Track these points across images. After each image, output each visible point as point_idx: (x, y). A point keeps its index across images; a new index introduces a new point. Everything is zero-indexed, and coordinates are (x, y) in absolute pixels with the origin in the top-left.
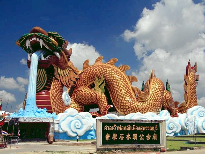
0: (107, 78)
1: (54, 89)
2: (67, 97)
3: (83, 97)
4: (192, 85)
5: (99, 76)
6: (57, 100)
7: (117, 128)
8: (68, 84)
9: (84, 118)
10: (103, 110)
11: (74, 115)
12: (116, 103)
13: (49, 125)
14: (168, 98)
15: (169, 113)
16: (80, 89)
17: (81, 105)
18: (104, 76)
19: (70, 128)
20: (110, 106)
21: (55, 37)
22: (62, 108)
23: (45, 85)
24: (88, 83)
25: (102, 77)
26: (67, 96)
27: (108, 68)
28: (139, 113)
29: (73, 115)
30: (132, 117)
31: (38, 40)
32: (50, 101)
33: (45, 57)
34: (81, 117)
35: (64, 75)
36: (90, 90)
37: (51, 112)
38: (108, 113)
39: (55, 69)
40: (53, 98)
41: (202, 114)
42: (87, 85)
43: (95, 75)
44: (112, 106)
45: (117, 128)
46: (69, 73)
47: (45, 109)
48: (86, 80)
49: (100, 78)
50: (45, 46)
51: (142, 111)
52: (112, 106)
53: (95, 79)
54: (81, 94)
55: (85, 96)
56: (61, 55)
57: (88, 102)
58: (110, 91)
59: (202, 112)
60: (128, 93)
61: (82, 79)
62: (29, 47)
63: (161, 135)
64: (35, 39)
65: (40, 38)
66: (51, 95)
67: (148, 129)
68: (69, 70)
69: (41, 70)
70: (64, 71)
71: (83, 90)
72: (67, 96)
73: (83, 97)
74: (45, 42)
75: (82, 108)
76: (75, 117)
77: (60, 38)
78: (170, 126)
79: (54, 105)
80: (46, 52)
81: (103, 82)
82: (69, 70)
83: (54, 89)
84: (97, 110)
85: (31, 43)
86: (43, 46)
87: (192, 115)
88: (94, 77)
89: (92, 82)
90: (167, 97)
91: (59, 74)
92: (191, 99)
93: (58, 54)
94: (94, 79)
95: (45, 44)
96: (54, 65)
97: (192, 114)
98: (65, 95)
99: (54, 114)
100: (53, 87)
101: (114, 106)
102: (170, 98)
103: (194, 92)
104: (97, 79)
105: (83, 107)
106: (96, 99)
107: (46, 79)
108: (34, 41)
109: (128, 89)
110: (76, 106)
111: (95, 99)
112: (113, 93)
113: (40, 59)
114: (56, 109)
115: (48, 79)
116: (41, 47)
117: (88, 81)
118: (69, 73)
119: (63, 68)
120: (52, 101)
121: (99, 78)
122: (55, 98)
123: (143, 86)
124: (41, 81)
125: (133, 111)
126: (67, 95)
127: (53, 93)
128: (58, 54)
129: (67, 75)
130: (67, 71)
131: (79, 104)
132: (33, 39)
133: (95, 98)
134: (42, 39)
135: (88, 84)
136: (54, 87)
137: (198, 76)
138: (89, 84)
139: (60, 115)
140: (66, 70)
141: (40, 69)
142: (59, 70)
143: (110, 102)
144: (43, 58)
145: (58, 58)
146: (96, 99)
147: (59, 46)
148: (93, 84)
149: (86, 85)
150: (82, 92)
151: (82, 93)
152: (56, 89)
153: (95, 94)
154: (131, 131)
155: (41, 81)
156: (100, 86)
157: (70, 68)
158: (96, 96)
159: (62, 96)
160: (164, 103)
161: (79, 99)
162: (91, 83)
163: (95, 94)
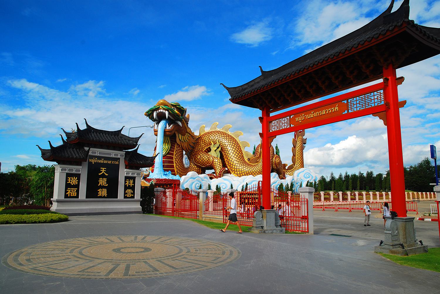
3: (201, 161)
4: (300, 149)
6: (179, 163)
7: (97, 161)
8: (188, 149)
9: (203, 179)
10: (218, 172)
11: (196, 177)
12: (230, 166)
14: (277, 162)
15: (277, 175)
16: (197, 153)
17: (198, 167)
20: (225, 169)
21: (389, 204)
22: (184, 171)
23: (169, 151)
26: (186, 160)
27: (223, 134)
28: (251, 176)
31: (164, 111)
34: (201, 179)
35: (184, 141)
40: (176, 162)
41: (307, 176)
42: (203, 149)
44: (226, 169)
45: (97, 161)
47: (170, 171)
48: (203, 145)
51: (253, 174)
52: (226, 169)
53: (211, 144)
54: (198, 157)
55: (202, 159)
56: (183, 123)
58: (225, 155)
59: (307, 174)
60: (242, 157)
61: (199, 144)
62: (168, 116)
63: (82, 217)
65: (166, 110)
67: (115, 163)
69: (168, 137)
70: (184, 137)
72: (186, 160)
73: (201, 161)
74: (169, 113)
75: (199, 170)
78: (198, 188)
79: (177, 168)
80: (170, 121)
81: (218, 148)
83: (177, 154)
84: (213, 171)
85: (158, 115)
87: (299, 176)
88: (210, 142)
89: (209, 147)
90: (276, 160)
91: (180, 140)
92: (298, 162)
93: (180, 124)
94: (210, 144)
96: (176, 133)
97: (298, 176)
98: (185, 160)
100: (176, 153)
101: (228, 169)
102: (279, 161)
103: (301, 153)
104: (213, 144)
105: (201, 169)
106: (213, 163)
107: (170, 146)
108: (161, 112)
109: (241, 154)
110: (196, 169)
112: (227, 157)
113: (165, 129)
114: (178, 172)
115: (171, 145)
117: (205, 145)
119: (183, 135)
120: (175, 165)
121: (215, 144)
123: (254, 149)
125: (244, 174)
126: (187, 158)
127: (176, 158)
128: (180, 124)
130: (186, 136)
132: (160, 111)
133: (211, 161)
134: (168, 110)
137: (306, 139)
138: (206, 148)
139: (183, 177)
140: (186, 135)
142: (180, 135)
143: (224, 165)
145: (180, 126)
146: (213, 163)
147: (182, 116)
148: (210, 148)
149: (202, 150)
150: (199, 156)
153: (211, 158)
154: (371, 189)
156: (215, 151)
157: (189, 133)
158: (212, 160)
159: (183, 160)
160: (274, 166)
161: (197, 162)
162: (207, 147)
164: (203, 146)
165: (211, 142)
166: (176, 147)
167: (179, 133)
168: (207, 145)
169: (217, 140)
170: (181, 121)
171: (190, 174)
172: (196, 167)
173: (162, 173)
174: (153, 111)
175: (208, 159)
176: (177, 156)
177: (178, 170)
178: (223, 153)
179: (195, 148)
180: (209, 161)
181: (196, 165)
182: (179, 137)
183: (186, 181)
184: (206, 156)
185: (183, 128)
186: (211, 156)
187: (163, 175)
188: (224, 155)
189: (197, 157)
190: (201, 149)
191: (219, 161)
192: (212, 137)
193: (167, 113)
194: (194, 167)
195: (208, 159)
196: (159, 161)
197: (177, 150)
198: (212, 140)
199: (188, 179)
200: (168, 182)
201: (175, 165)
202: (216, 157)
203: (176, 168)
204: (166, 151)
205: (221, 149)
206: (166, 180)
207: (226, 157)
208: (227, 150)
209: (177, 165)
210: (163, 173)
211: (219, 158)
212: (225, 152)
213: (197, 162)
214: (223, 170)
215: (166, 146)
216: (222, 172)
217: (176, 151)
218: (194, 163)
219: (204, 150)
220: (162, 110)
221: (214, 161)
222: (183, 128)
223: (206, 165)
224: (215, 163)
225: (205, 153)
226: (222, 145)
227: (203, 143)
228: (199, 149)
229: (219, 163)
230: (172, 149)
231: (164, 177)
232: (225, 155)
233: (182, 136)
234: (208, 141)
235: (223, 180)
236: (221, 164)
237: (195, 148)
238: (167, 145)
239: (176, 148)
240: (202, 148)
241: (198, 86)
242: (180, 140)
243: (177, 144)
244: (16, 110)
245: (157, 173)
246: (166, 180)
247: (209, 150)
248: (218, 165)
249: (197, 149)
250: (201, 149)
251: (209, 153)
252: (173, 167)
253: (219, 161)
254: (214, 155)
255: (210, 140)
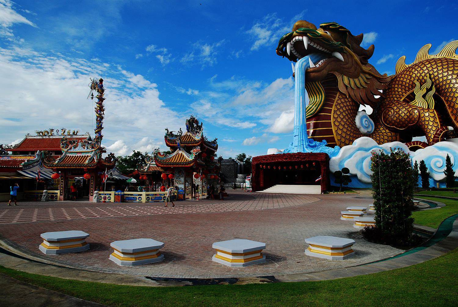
0: (438, 79)
1: (338, 109)
2: (366, 121)
5: (423, 78)
13: (289, 155)
16: (388, 106)
17: (392, 131)
18: (432, 76)
19: (361, 169)
20: (447, 129)
24: (404, 94)
25: (428, 80)
26: (364, 119)
29: (367, 147)
30: (357, 86)
31: (300, 38)
32: (331, 128)
33: (315, 64)
36: (404, 103)
37: (333, 146)
38: (443, 140)
39: (339, 79)
42: (401, 98)
43: (414, 79)
44: (450, 128)
46: (366, 83)
47: (324, 141)
48: (400, 90)
49: (425, 81)
50: (317, 48)
53: (416, 85)
54: (390, 113)
57: (404, 125)
64: (297, 38)
66: (332, 120)
68: (367, 78)
69: (317, 83)
70: (356, 80)
71: (394, 107)
74: (310, 39)
76: (371, 150)
77: (340, 29)
81: (431, 89)
82: (367, 78)
83: (338, 109)
86: (309, 45)
88: (413, 83)
89: (411, 91)
93: (339, 56)
94: (414, 85)
95: (312, 42)
99: (337, 147)
104: (418, 84)
110: (389, 134)
111: (417, 119)
115: (326, 96)
116: (306, 49)
117: (404, 91)
118: (366, 83)
120: (334, 129)
122: (340, 122)
124: (316, 101)
127: (336, 116)
128: (339, 56)
129: (362, 86)
131: (389, 130)
132: (294, 39)
135: (403, 96)
136: (338, 107)
138: (405, 95)
139: (344, 148)
140: (360, 78)
141: (311, 83)
142: (346, 78)
144: (312, 65)
145: (341, 61)
150: (392, 111)
151: (392, 112)
152: (341, 111)
153: (416, 111)
155: (316, 101)
156: (424, 96)
158: (418, 114)
162: (408, 93)
163: (416, 111)
164: (401, 93)
165: (415, 81)
166: (337, 98)
167: (343, 73)
168: (407, 89)
169: (428, 75)
170: (341, 52)
171: (358, 142)
172: (387, 131)
173: (306, 143)
174: (284, 42)
175: (408, 114)
176: (345, 115)
177: (342, 137)
178: (443, 99)
179: (385, 98)
180: (411, 117)
181: (387, 128)
182: (343, 80)
183: (348, 155)
184: (404, 109)
185: (349, 65)
186: (415, 107)
187: (307, 147)
188: (445, 103)
189: (388, 113)
190: (395, 99)
191: (432, 115)
192: (416, 73)
193: (305, 39)
194: (384, 131)
195: (408, 114)
196: (298, 125)
197: (339, 104)
198: (417, 78)
199: (352, 151)
200: (304, 158)
201: (335, 128)
202: (427, 108)
203: (337, 134)
204: (316, 107)
205: (437, 90)
206: (301, 155)
207: (449, 106)
208: (450, 90)
209: (338, 128)
210: (307, 144)
211: (433, 108)
212: (446, 96)
213: (388, 122)
214: (441, 132)
215: (317, 98)
216: (439, 135)
217: (336, 105)
218: (385, 125)
219: (402, 100)
220: (297, 38)
221: (422, 115)
222: (349, 65)
223: (407, 125)
224: (423, 119)
225: (404, 103)
226: (439, 84)
227: (400, 86)
228: (392, 99)
229: (432, 119)
230: (328, 102)
231: (308, 151)
232: (447, 101)
233: (351, 80)
234: (408, 81)
235: (437, 150)
236: (438, 121)
237: (385, 98)
238: (318, 97)
239: (338, 100)
240: (398, 96)
241: (444, 43)
242: (346, 87)
243: (340, 92)
244: (280, 118)
245: (297, 144)
246: (301, 155)
247: (412, 97)
248: (431, 123)
249: (389, 99)
250: (395, 99)
251: (412, 103)
252: (330, 132)
253: (432, 115)
254: (422, 106)
255: (412, 79)
